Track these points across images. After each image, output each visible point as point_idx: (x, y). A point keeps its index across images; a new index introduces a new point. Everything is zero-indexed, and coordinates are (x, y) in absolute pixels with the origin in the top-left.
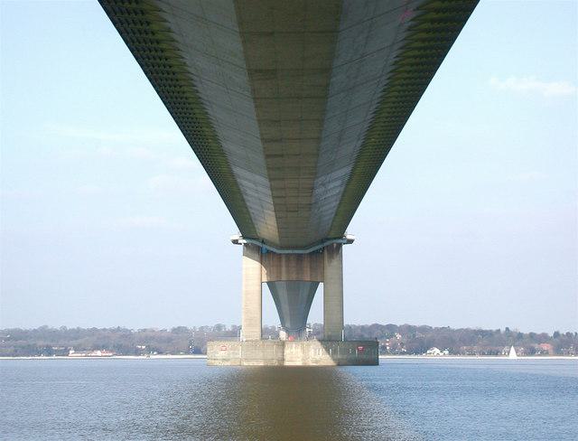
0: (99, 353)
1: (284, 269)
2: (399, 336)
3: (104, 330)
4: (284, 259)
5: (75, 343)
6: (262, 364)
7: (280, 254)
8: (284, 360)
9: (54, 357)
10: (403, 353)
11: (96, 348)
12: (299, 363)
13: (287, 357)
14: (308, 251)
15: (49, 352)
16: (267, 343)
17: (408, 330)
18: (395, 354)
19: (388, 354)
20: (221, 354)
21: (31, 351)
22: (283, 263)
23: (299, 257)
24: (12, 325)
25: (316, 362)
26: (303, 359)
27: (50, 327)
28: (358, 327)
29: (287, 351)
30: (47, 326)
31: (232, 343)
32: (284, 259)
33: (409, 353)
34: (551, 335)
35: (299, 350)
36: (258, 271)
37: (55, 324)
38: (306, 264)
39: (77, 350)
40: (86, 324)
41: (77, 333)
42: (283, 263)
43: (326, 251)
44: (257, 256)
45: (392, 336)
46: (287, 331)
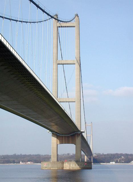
0: (29, 163)
1: (64, 140)
2: (123, 157)
3: (33, 155)
4: (64, 138)
5: (22, 159)
6: (57, 169)
7: (63, 136)
8: (63, 167)
9: (15, 164)
10: (123, 163)
11: (28, 161)
12: (68, 168)
13: (64, 167)
14: (70, 135)
15: (14, 162)
16: (58, 162)
17: (127, 155)
18: (120, 163)
19: (118, 163)
20: (45, 166)
21: (9, 162)
22: (64, 139)
23: (68, 137)
24: (5, 154)
25: (73, 168)
26: (69, 167)
27: (17, 154)
28: (115, 154)
29: (64, 165)
30: (16, 154)
31: (48, 162)
32: (64, 138)
33: (125, 162)
34: (94, 165)
35: (68, 164)
36: (56, 141)
37: (18, 153)
38: (70, 139)
39: (22, 162)
40: (28, 153)
41: (25, 156)
42: (64, 139)
43: (76, 135)
44: (56, 137)
45: (121, 157)
46: (87, 156)
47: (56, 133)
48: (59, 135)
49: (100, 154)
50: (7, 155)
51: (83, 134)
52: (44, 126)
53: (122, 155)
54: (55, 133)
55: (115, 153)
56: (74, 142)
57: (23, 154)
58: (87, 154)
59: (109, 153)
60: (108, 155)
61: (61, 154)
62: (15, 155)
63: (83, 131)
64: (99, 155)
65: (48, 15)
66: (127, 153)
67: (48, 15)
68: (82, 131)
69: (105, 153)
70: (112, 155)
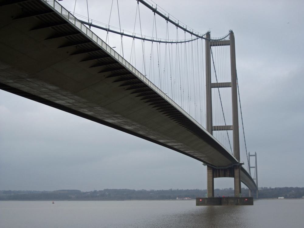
2: (293, 191)
17: (297, 189)
27: (173, 190)
30: (172, 189)
41: (181, 191)
47: (211, 165)
48: (216, 168)
49: (267, 188)
50: (163, 190)
51: (243, 166)
52: (167, 142)
53: (292, 189)
54: (210, 166)
55: (284, 186)
56: (232, 175)
57: (289, 186)
58: (151, 193)
59: (277, 187)
60: (276, 189)
61: (222, 189)
62: (171, 190)
63: (242, 163)
64: (266, 189)
65: (192, 33)
66: (106, 189)
67: (192, 33)
68: (241, 162)
69: (273, 187)
70: (280, 189)
